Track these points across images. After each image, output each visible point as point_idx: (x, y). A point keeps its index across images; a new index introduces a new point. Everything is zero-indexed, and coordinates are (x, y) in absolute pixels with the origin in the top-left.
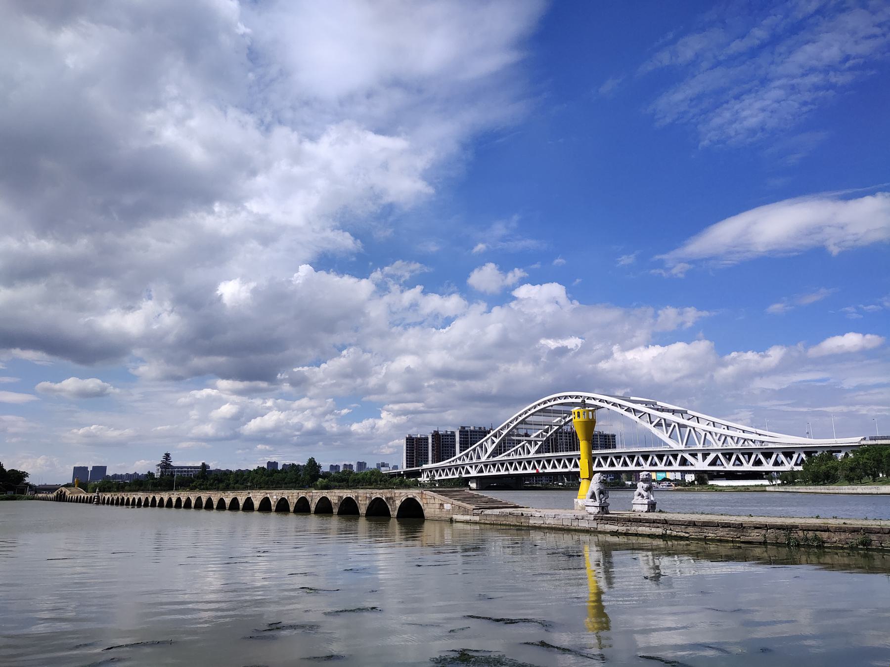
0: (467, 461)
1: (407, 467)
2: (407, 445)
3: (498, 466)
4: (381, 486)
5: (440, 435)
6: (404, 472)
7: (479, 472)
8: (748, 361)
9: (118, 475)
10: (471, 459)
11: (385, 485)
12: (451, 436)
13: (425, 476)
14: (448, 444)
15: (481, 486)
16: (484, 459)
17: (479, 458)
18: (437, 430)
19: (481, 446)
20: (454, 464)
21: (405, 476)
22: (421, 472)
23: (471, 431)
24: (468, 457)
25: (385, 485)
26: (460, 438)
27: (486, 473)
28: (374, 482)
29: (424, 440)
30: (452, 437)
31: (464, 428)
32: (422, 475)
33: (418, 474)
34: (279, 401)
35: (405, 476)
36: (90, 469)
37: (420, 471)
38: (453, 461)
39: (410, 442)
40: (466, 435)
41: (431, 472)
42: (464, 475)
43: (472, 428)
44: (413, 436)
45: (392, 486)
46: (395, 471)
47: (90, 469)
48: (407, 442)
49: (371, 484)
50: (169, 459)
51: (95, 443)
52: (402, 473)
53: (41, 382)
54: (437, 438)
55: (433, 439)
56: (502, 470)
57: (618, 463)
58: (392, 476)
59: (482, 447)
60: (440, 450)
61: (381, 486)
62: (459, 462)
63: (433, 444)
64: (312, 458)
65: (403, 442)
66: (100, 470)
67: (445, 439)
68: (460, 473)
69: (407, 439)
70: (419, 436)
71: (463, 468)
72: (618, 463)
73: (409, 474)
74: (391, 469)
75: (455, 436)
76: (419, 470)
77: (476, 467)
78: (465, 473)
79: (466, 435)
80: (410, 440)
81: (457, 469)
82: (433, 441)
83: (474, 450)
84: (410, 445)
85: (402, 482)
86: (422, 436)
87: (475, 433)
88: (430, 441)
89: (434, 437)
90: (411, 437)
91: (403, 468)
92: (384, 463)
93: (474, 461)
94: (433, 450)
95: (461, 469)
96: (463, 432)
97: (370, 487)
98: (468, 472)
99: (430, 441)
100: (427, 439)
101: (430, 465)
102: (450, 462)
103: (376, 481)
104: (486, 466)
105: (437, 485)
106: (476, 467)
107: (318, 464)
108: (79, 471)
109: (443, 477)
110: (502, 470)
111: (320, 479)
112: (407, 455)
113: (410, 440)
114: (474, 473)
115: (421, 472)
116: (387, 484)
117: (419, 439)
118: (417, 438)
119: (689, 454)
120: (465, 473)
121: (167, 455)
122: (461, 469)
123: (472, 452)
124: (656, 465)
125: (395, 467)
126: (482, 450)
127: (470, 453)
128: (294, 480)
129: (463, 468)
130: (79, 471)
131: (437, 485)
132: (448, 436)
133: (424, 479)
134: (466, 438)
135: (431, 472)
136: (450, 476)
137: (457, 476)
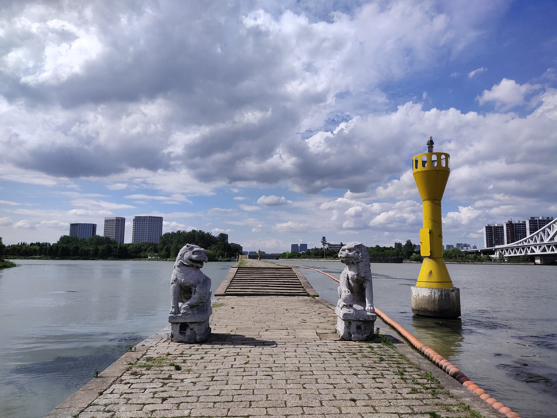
0: (532, 243)
1: (487, 247)
2: (486, 231)
3: (526, 249)
4: (459, 260)
5: (513, 224)
6: (481, 250)
7: (542, 251)
8: (345, 200)
9: (386, 248)
10: (536, 241)
11: (462, 259)
12: (523, 224)
13: (498, 253)
14: (520, 231)
15: (544, 262)
16: (546, 241)
17: (542, 240)
18: (510, 221)
19: (544, 231)
20: (521, 245)
21: (482, 253)
22: (494, 251)
23: (539, 221)
24: (532, 240)
25: (462, 259)
26: (530, 226)
27: (549, 252)
28: (454, 257)
29: (501, 228)
30: (524, 226)
31: (533, 218)
32: (496, 253)
33: (493, 252)
34: (415, 202)
35: (482, 253)
36: (299, 246)
37: (494, 250)
38: (520, 243)
39: (489, 230)
40: (535, 224)
41: (502, 251)
42: (529, 253)
43: (541, 218)
44: (492, 225)
45: (468, 260)
46: (474, 250)
47: (299, 246)
48: (486, 229)
49: (451, 258)
50: (325, 240)
51: (292, 231)
52: (479, 251)
53: (238, 196)
54: (511, 226)
55: (507, 227)
56: (518, 252)
57: (549, 250)
58: (467, 253)
59: (545, 233)
60: (514, 235)
61: (459, 260)
62: (525, 244)
63: (507, 231)
64: (409, 240)
65: (484, 230)
66: (304, 246)
67: (518, 227)
68: (527, 252)
69: (486, 227)
70: (496, 225)
71: (529, 248)
72: (549, 250)
73: (485, 252)
74: (472, 248)
75: (525, 224)
76: (493, 249)
77: (540, 247)
78: (531, 252)
79: (535, 224)
80: (489, 228)
81: (523, 249)
82: (507, 229)
83: (537, 234)
84: (489, 232)
85: (475, 258)
86: (499, 225)
87: (543, 222)
88: (505, 228)
89: (507, 226)
90: (490, 226)
91: (485, 247)
92: (466, 244)
93: (538, 242)
94: (507, 235)
95: (527, 249)
96: (510, 225)
97: (450, 260)
98: (533, 251)
99: (505, 228)
100: (502, 227)
101: (506, 245)
102: (518, 244)
103: (455, 257)
104: (549, 247)
105: (506, 261)
106: (540, 247)
107: (413, 244)
108: (294, 247)
109: (513, 255)
110: (518, 252)
111: (414, 254)
112: (487, 239)
113: (489, 228)
114: (538, 252)
115: (494, 251)
116: (464, 258)
117: (497, 228)
118: (495, 227)
119: (534, 247)
120: (531, 252)
121: (324, 238)
122: (527, 249)
123: (536, 236)
124: (546, 251)
125: (475, 247)
126: (545, 235)
127: (534, 237)
128: (396, 254)
129: (529, 248)
130: (294, 247)
131: (506, 261)
132: (520, 224)
133: (496, 256)
134: (535, 226)
135: (502, 251)
136: (518, 254)
137: (523, 254)
